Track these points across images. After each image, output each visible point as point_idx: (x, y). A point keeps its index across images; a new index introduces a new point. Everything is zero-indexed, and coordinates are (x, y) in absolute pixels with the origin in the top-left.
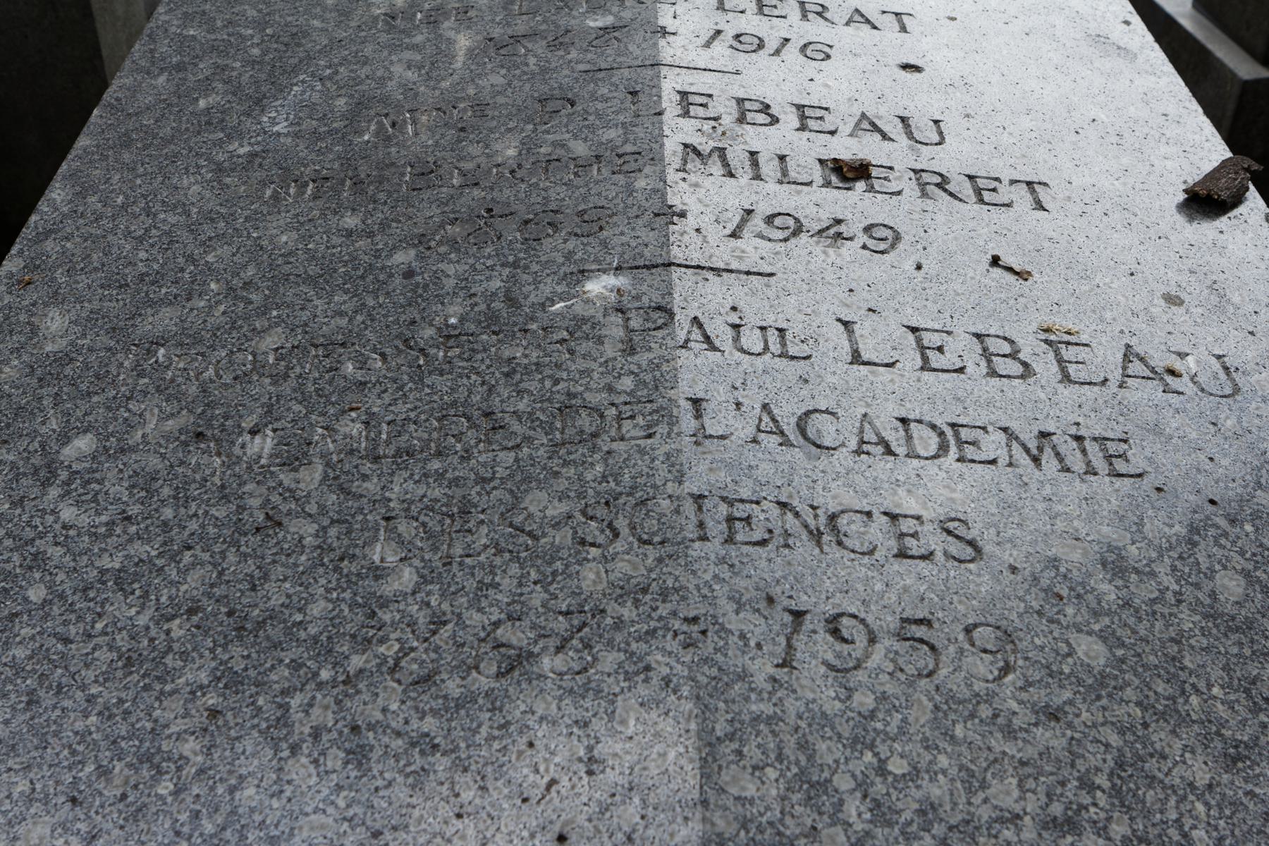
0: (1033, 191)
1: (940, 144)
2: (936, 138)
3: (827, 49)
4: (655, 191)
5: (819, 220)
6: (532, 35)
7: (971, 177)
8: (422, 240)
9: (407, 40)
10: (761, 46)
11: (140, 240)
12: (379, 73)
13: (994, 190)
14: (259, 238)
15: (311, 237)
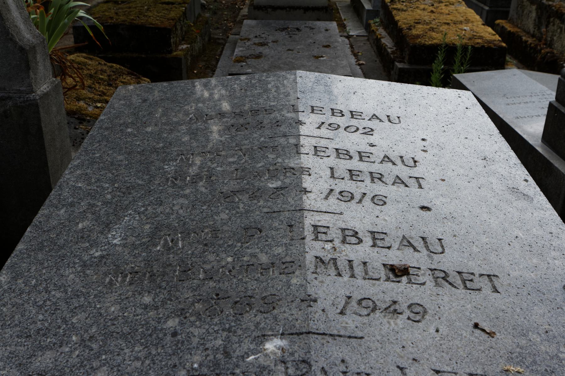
0: (491, 281)
1: (442, 253)
2: (440, 250)
3: (384, 199)
4: (302, 286)
5: (385, 302)
6: (241, 191)
7: (459, 273)
8: (182, 313)
9: (181, 192)
10: (352, 198)
11: (40, 307)
12: (167, 211)
13: (471, 280)
14: (100, 308)
15: (126, 308)
